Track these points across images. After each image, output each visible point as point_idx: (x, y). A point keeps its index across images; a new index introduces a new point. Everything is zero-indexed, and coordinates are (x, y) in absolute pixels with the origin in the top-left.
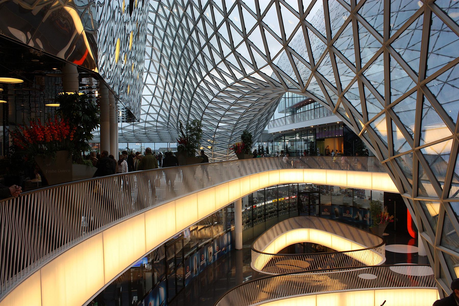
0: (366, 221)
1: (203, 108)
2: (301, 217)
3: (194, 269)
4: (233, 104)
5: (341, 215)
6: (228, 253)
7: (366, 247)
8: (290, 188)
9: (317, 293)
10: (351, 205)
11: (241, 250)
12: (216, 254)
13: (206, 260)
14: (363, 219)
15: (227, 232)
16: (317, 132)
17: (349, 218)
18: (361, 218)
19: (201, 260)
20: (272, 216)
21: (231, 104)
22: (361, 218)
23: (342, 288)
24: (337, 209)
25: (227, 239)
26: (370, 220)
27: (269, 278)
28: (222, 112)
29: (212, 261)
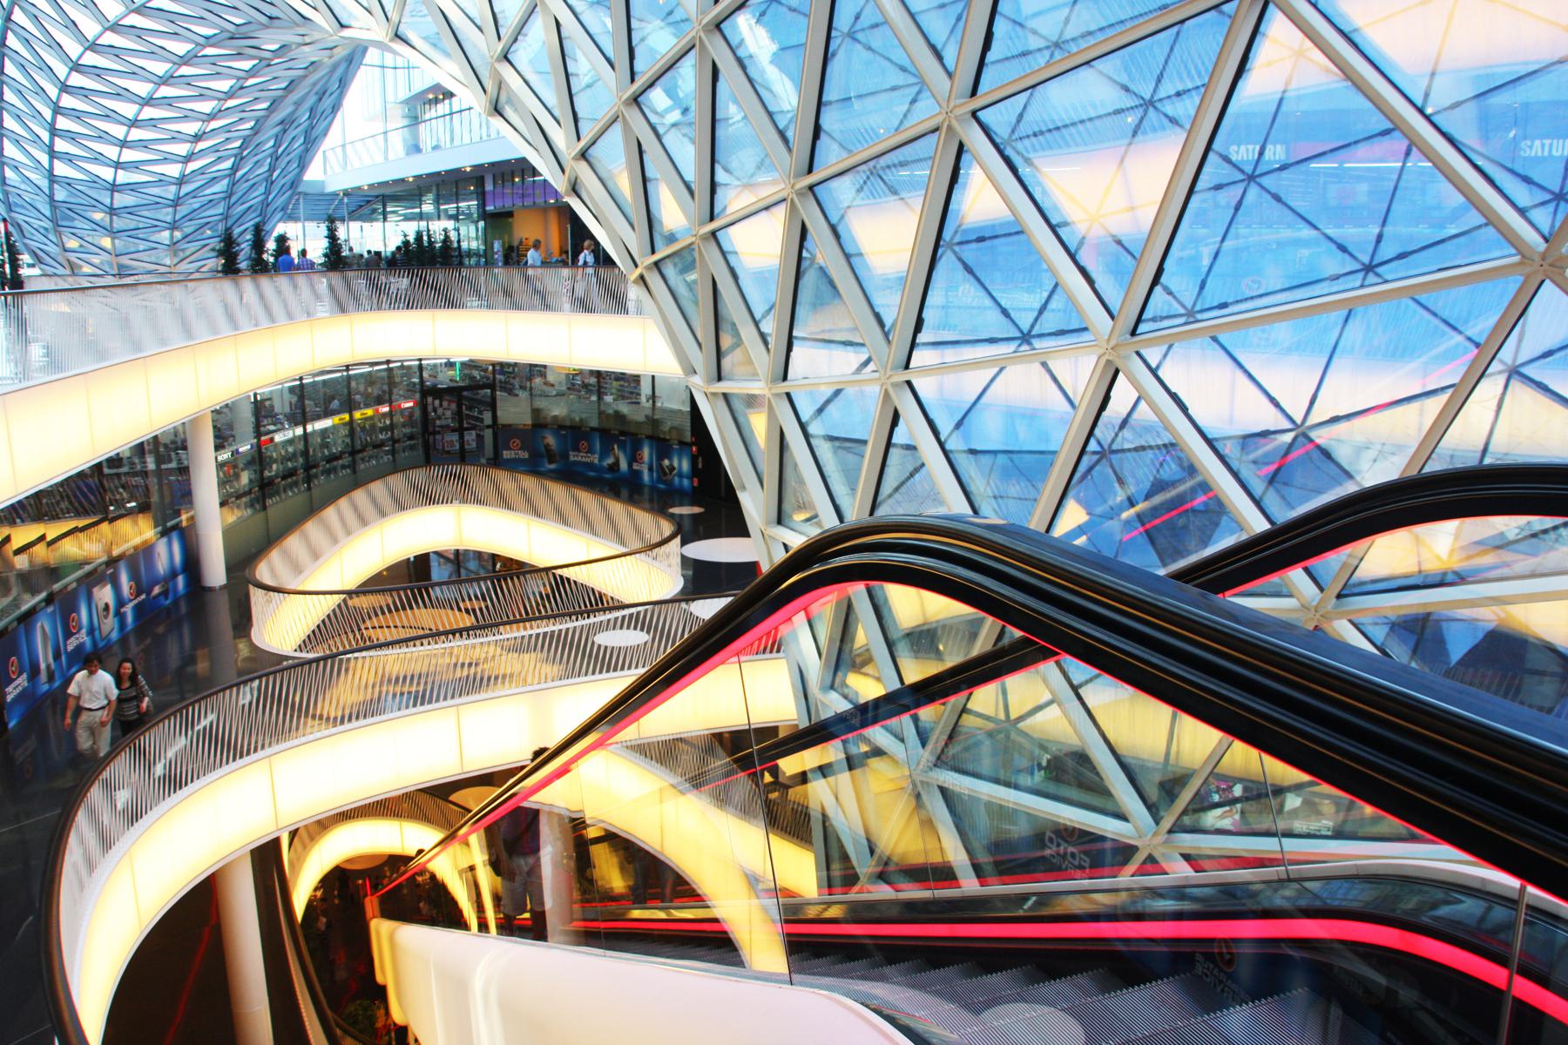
0: (638, 474)
1: (53, 92)
2: (436, 471)
3: (43, 666)
4: (185, 60)
5: (565, 456)
6: (176, 602)
7: (624, 550)
8: (385, 381)
9: (457, 700)
10: (594, 423)
11: (223, 588)
12: (128, 610)
13: (91, 632)
14: (630, 465)
15: (165, 533)
16: (489, 187)
17: (590, 466)
18: (624, 466)
19: (68, 634)
20: (334, 470)
21: (176, 60)
22: (624, 466)
23: (352, 663)
24: (551, 440)
25: (167, 555)
26: (651, 469)
27: (294, 666)
28: (142, 89)
29: (115, 635)
